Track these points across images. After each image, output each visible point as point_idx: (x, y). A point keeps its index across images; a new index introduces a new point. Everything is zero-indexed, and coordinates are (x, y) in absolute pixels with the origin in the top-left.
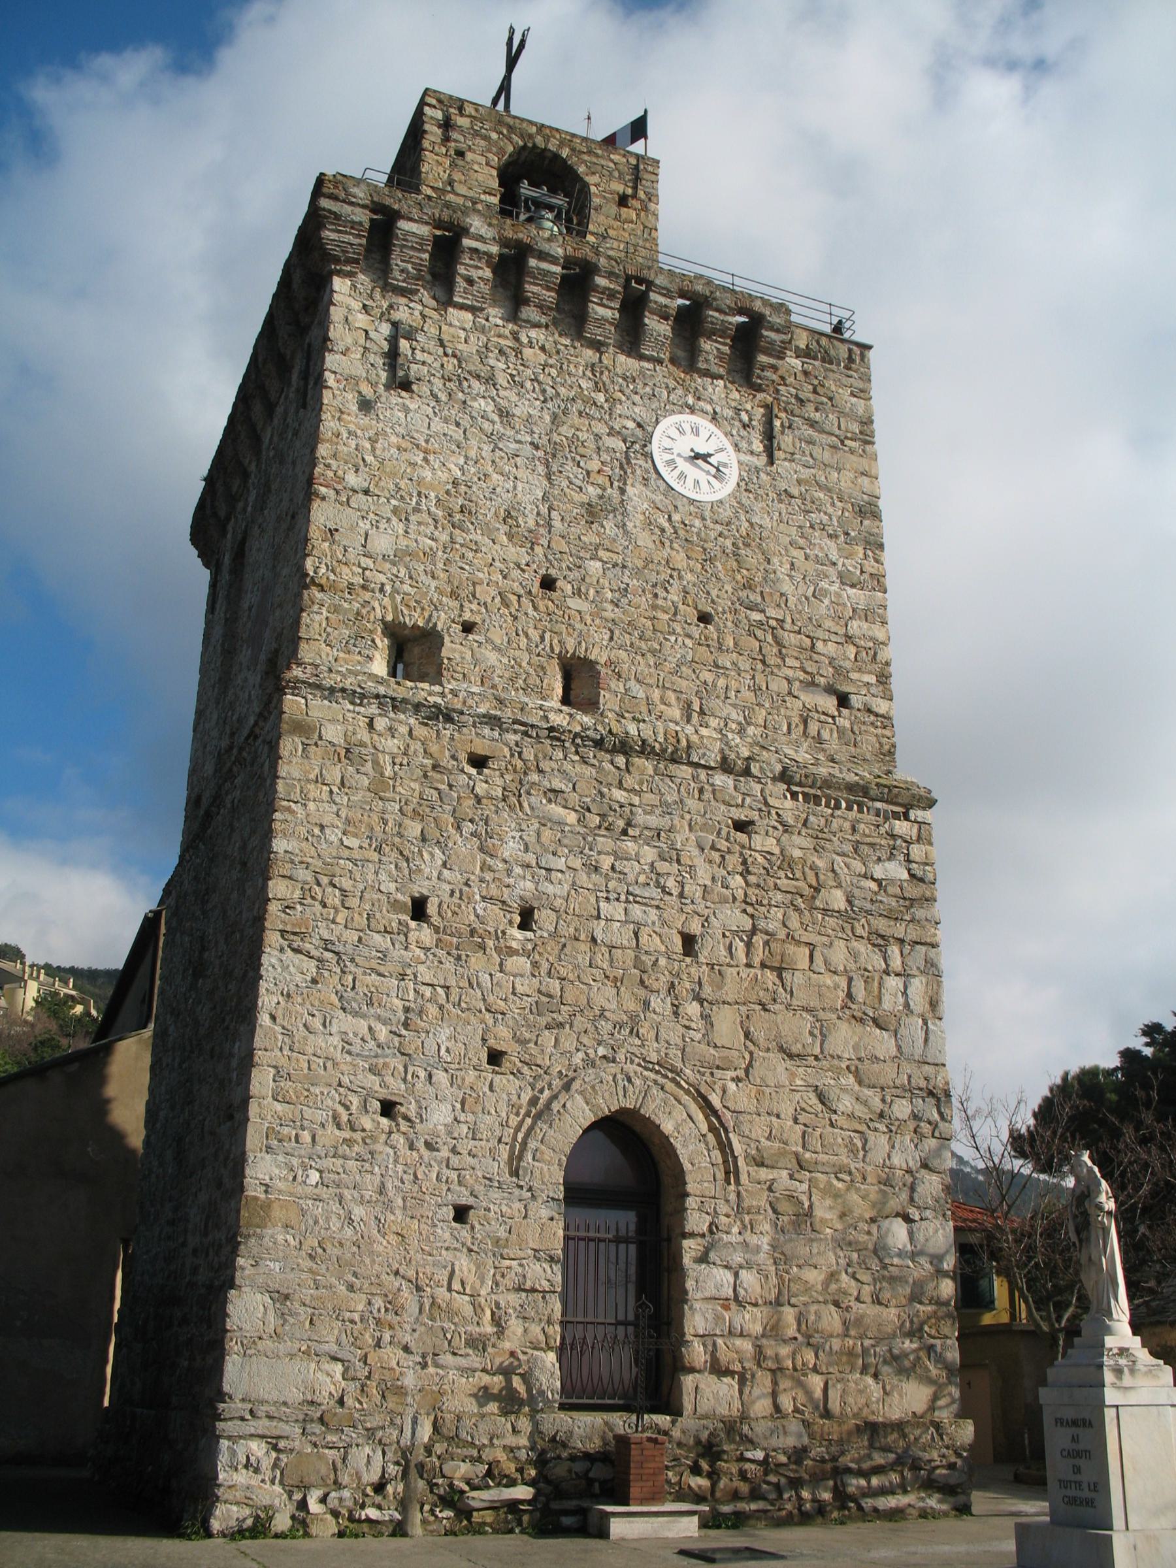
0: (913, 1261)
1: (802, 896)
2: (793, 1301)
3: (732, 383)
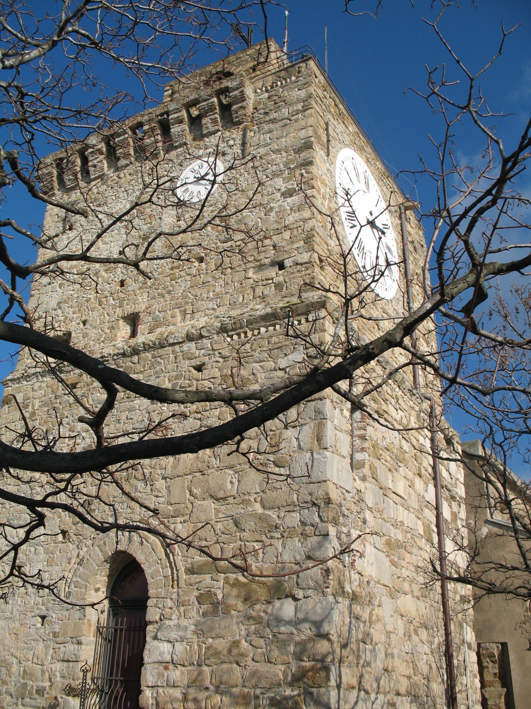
0: (297, 629)
2: (207, 662)
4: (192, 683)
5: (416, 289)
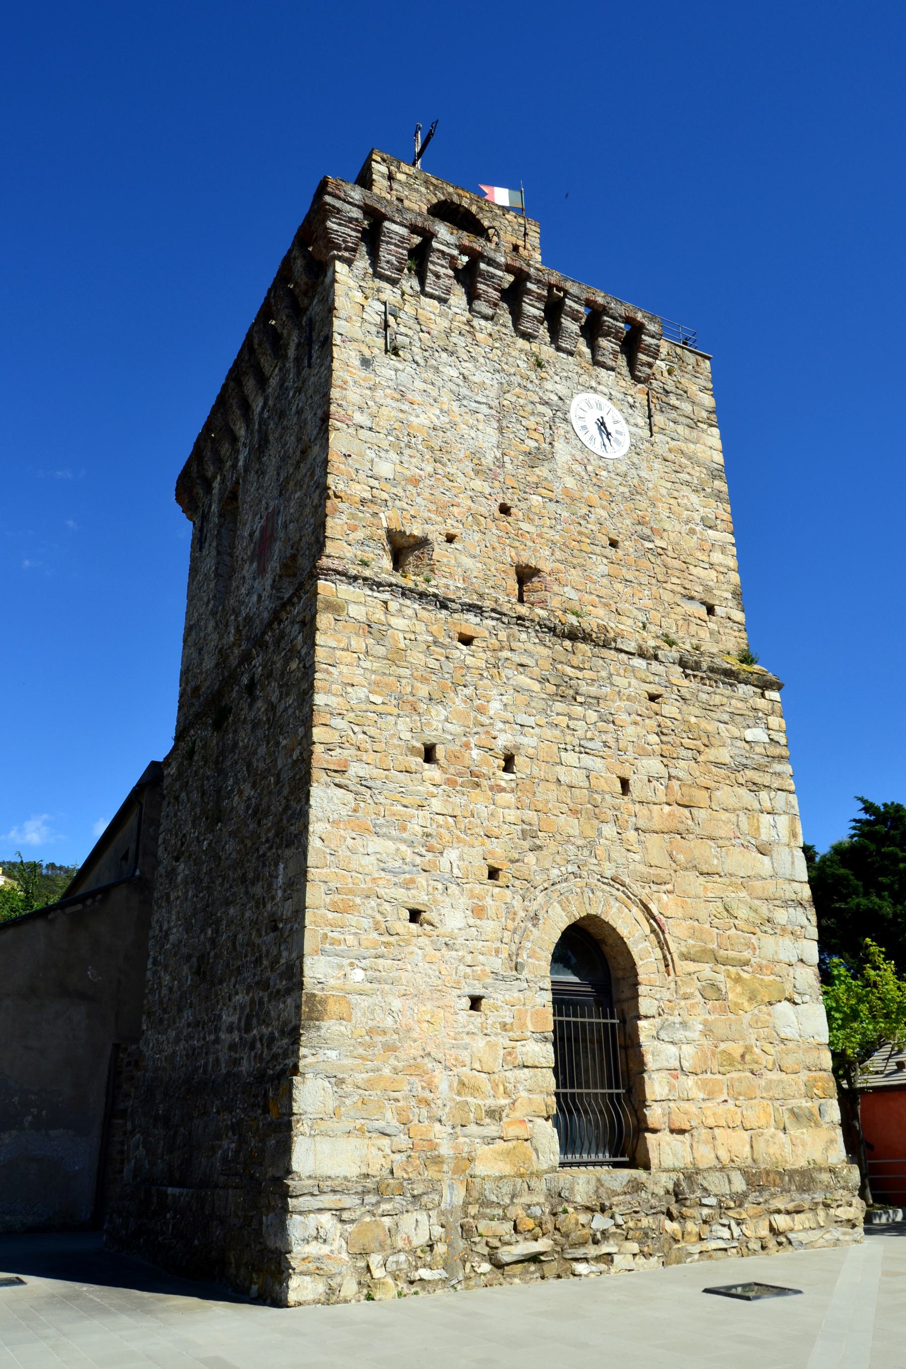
5: (536, 304)
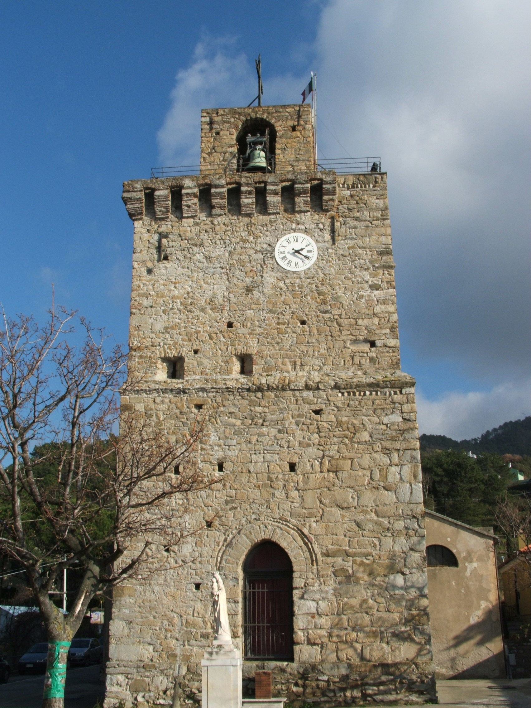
0: (406, 592)
1: (347, 438)
2: (345, 613)
3: (315, 212)
4: (335, 626)
